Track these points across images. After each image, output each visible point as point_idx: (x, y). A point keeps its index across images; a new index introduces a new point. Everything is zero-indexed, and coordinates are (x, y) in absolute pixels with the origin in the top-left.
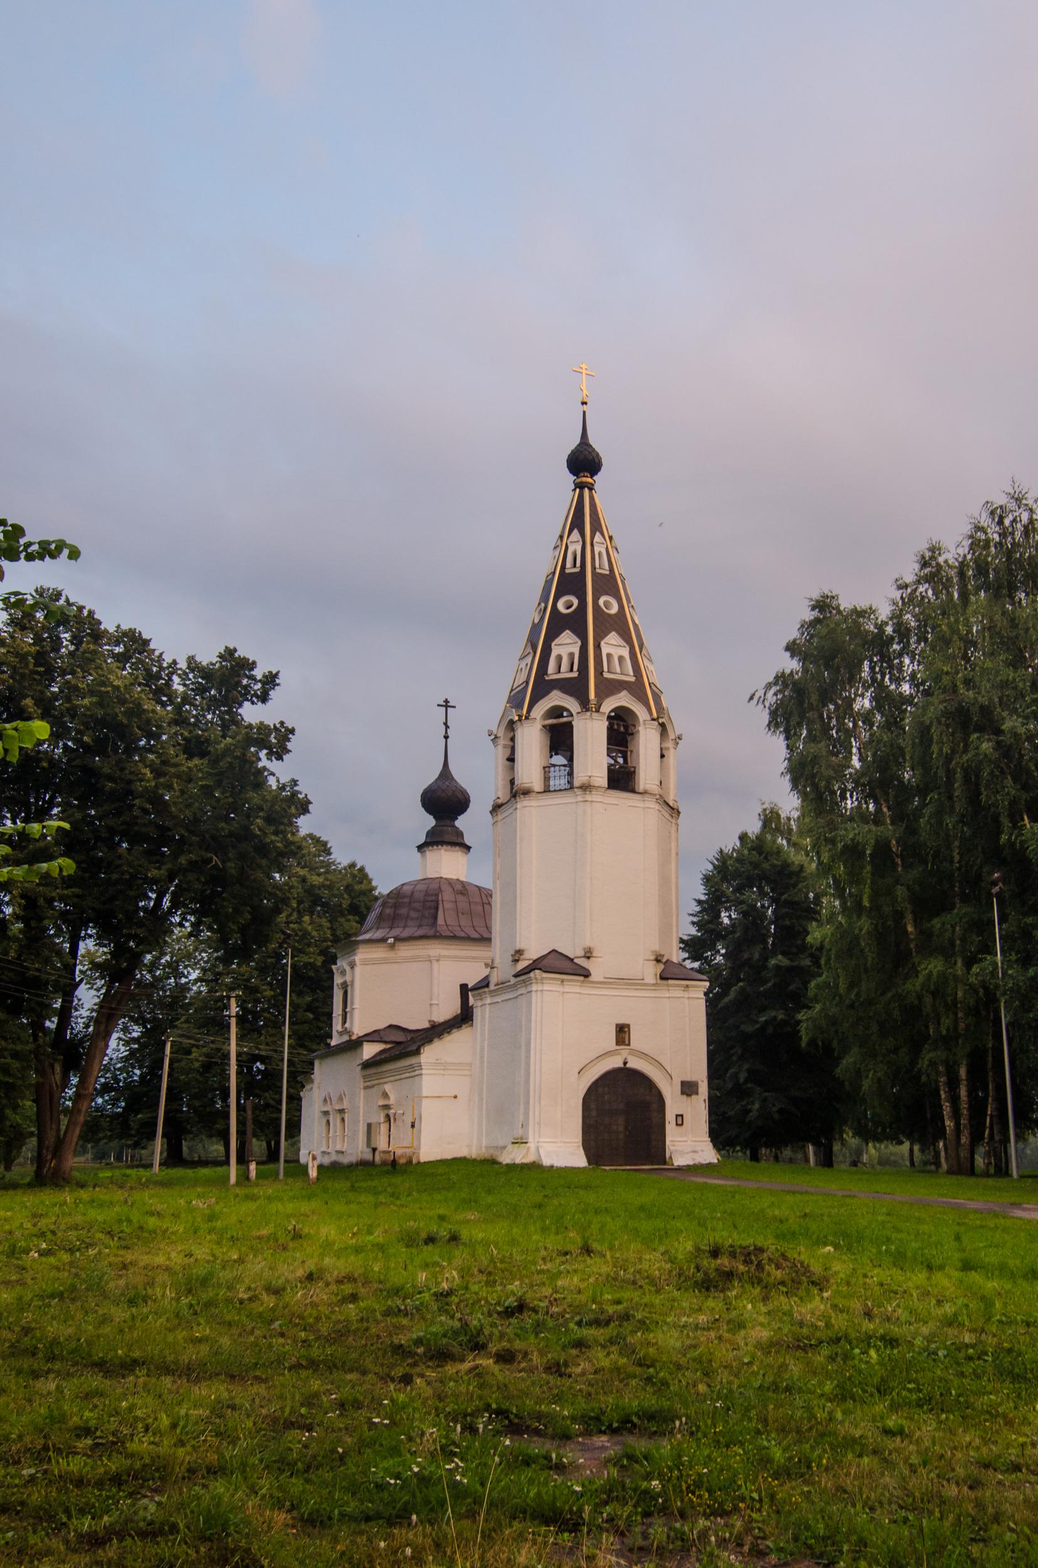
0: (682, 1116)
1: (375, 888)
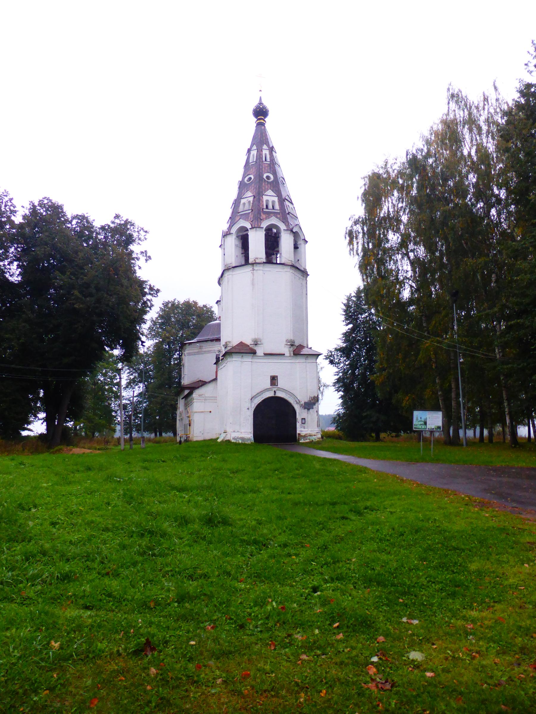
1: (342, 397)
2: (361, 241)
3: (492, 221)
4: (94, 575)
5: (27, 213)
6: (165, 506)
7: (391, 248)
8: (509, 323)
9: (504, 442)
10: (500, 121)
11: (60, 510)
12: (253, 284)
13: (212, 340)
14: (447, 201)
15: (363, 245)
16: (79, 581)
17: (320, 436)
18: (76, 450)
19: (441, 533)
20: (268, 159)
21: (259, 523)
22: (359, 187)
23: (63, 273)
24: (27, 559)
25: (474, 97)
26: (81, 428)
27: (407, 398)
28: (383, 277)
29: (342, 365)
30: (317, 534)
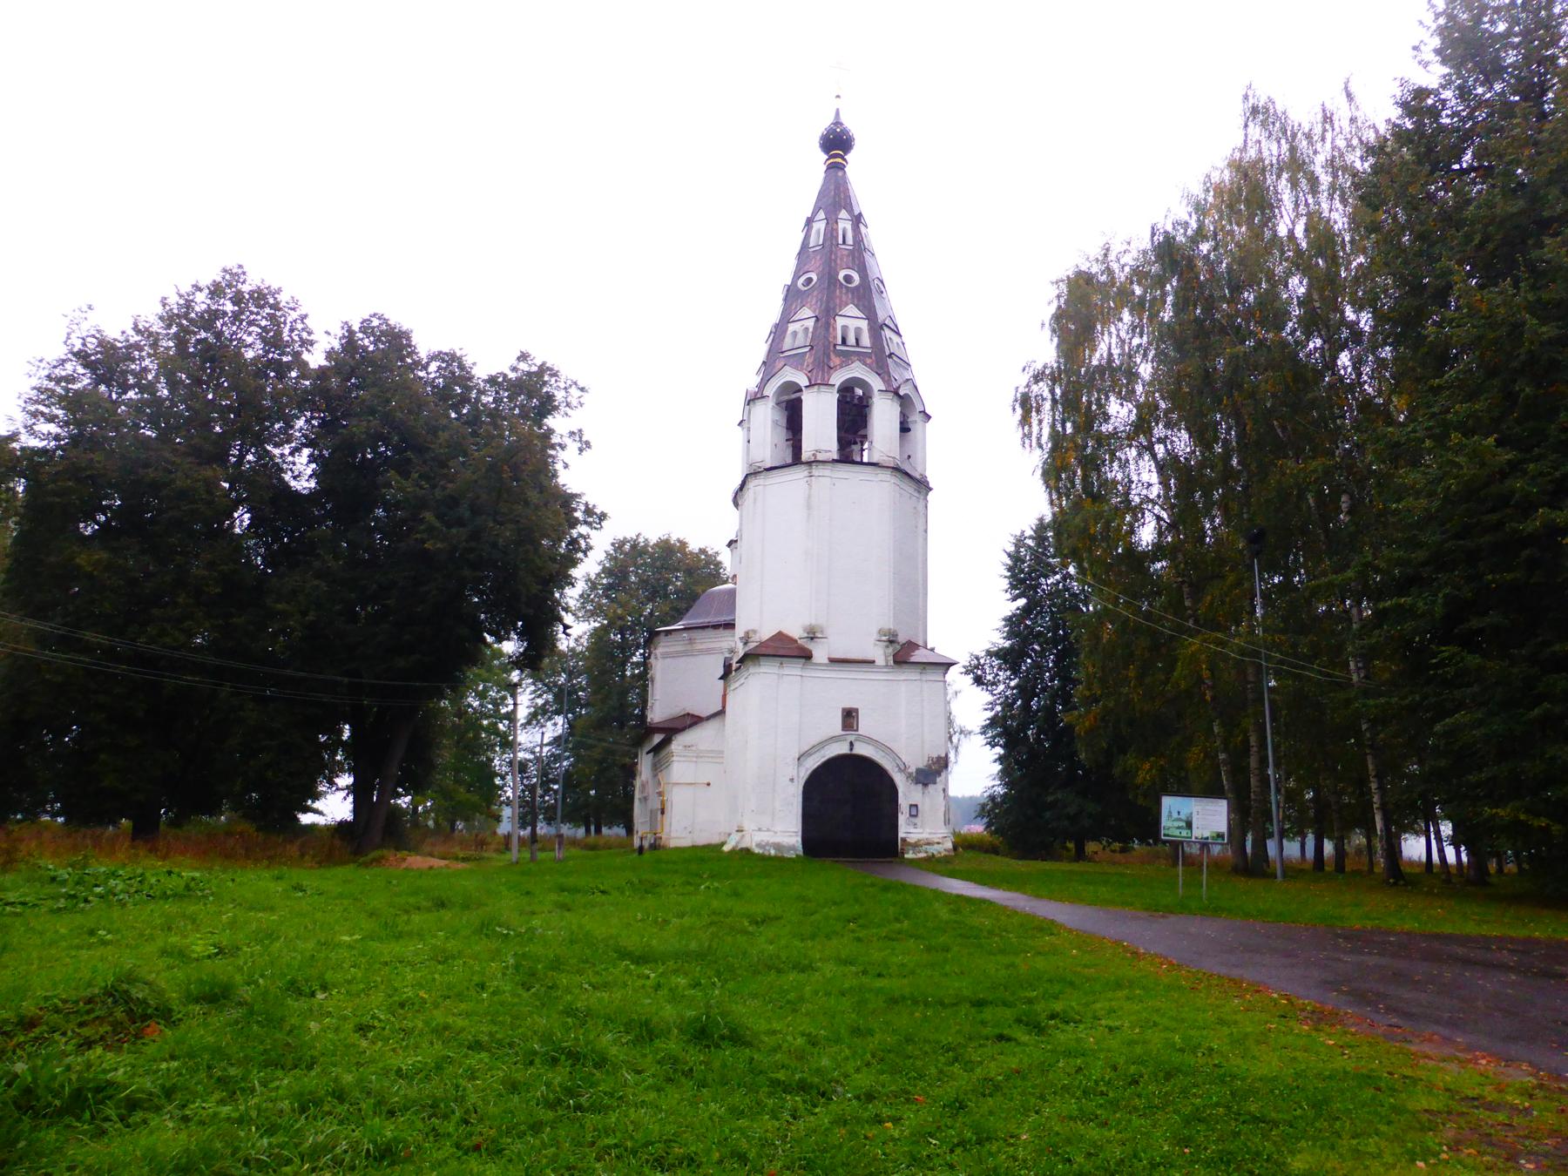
1: (1001, 759)
2: (1047, 418)
3: (1341, 379)
4: (448, 1149)
5: (337, 345)
6: (605, 995)
7: (1114, 434)
8: (1381, 605)
9: (1371, 871)
10: (1358, 164)
11: (378, 998)
12: (809, 507)
13: (716, 627)
14: (1240, 335)
15: (1053, 426)
16: (413, 1163)
17: (949, 845)
18: (416, 861)
19: (1223, 1082)
20: (850, 240)
21: (813, 1042)
22: (1045, 302)
23: (405, 474)
24: (303, 1109)
25: (1303, 115)
26: (426, 811)
27: (1147, 766)
28: (1096, 498)
29: (1001, 687)
30: (941, 1072)
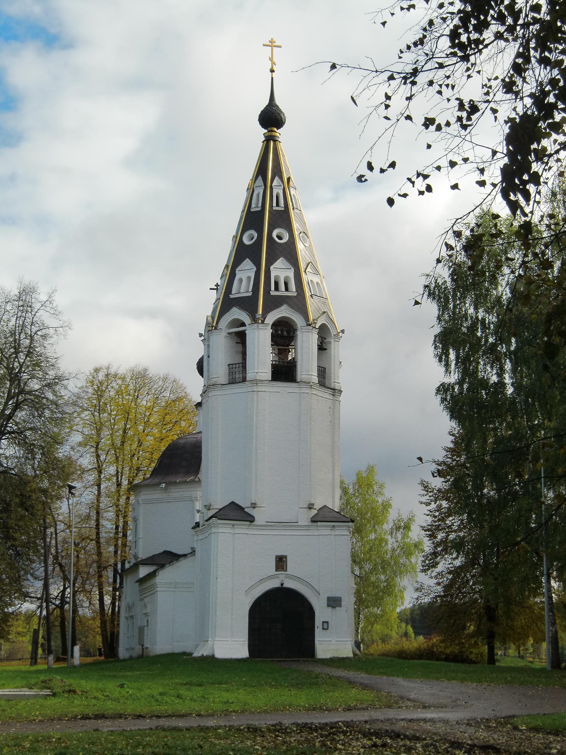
0: (327, 622)
